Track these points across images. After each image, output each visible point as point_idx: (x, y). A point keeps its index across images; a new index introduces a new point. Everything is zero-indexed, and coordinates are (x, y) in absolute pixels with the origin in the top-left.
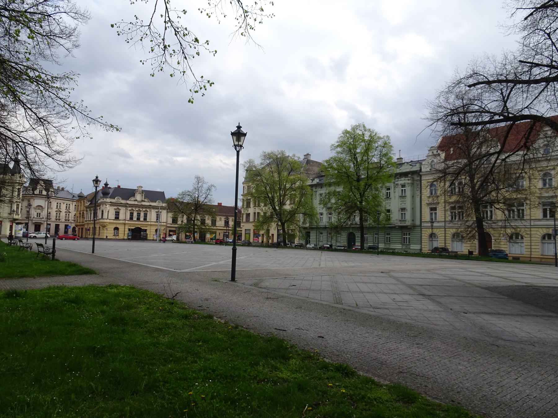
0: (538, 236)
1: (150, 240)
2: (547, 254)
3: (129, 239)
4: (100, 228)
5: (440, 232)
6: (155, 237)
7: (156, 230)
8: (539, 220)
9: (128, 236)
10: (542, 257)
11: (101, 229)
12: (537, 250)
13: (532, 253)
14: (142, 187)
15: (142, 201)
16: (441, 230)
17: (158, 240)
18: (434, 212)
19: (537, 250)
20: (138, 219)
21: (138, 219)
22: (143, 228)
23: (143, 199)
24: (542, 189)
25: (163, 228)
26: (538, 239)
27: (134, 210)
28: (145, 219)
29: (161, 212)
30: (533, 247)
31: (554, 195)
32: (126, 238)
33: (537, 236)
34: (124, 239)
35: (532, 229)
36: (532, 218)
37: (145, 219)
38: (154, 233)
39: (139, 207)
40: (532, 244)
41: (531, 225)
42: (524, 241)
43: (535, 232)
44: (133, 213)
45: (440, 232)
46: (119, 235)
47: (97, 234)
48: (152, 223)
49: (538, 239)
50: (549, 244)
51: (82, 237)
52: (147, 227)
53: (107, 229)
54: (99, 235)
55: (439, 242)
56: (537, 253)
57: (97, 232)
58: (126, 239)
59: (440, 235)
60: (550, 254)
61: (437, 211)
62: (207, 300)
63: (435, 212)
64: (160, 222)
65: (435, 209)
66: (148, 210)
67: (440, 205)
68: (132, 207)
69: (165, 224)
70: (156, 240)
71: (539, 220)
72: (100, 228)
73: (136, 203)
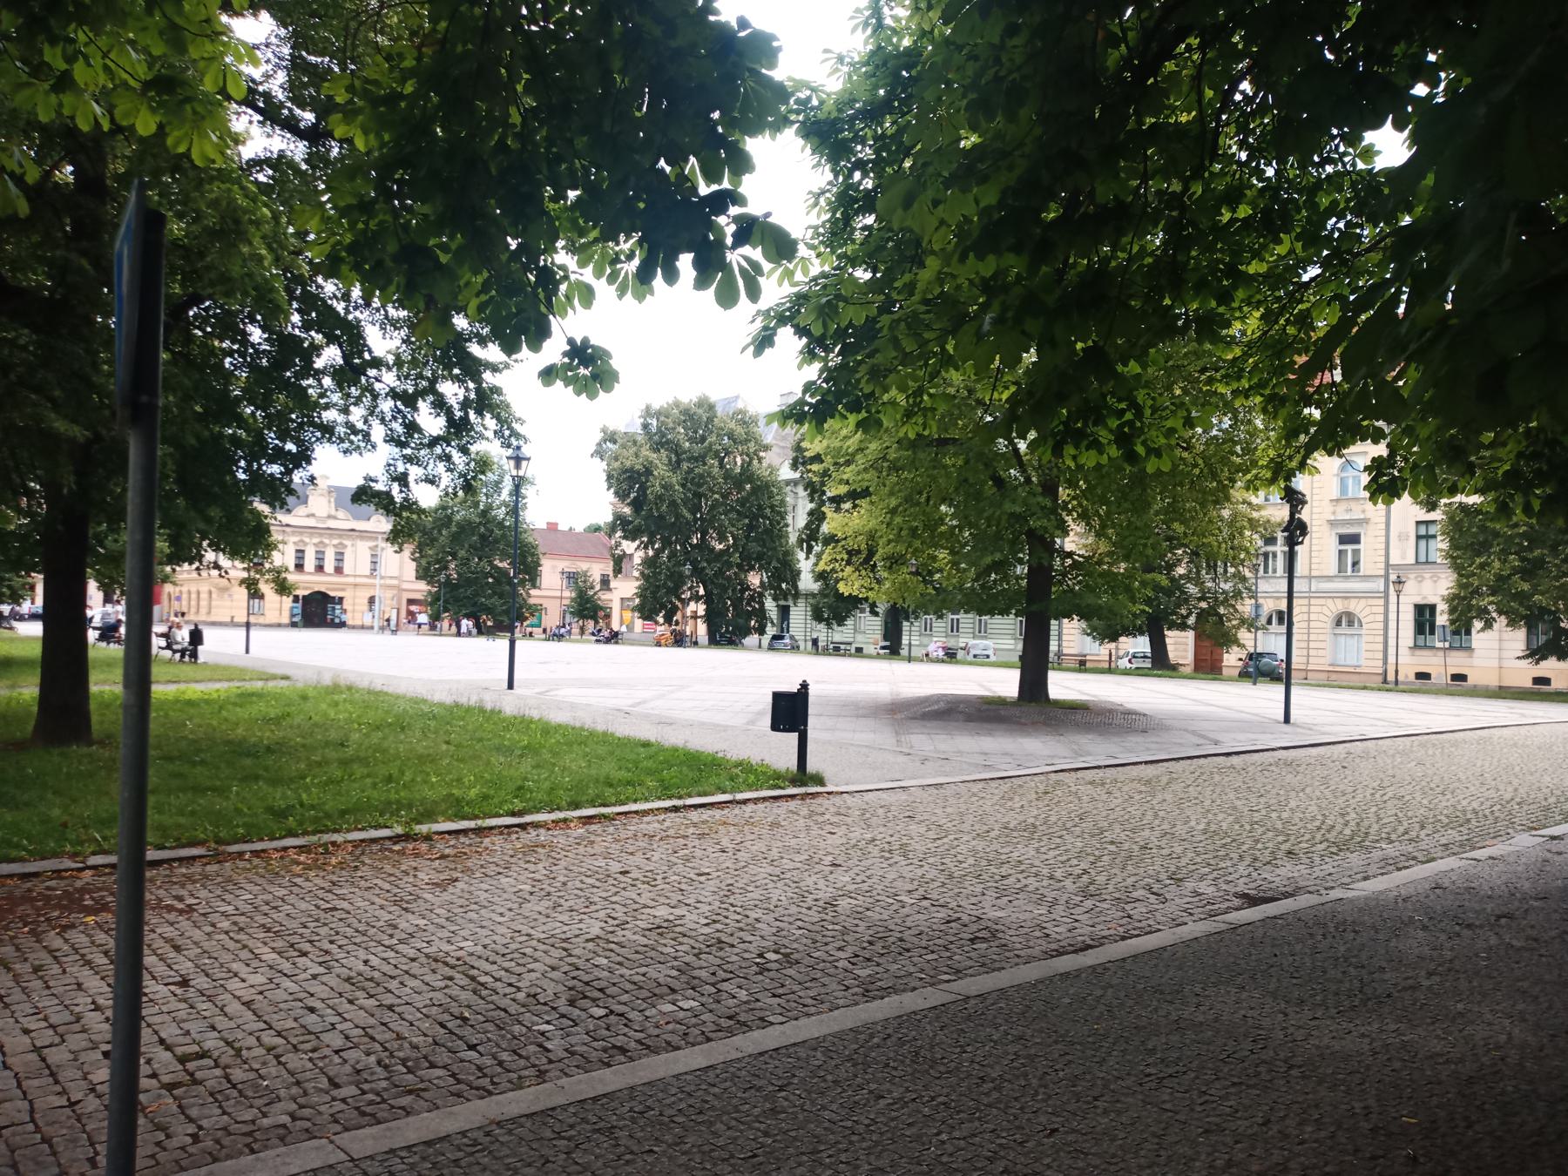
0: (1326, 619)
1: (354, 627)
2: (1342, 663)
3: (294, 625)
4: (210, 593)
5: (1368, 610)
6: (367, 620)
7: (372, 600)
8: (1329, 578)
9: (293, 616)
10: (1331, 669)
11: (214, 596)
12: (1321, 653)
13: (1312, 660)
14: (327, 478)
15: (330, 517)
16: (1371, 602)
17: (376, 628)
18: (1349, 548)
19: (1321, 653)
20: (320, 568)
21: (320, 568)
22: (332, 594)
23: (333, 512)
24: (1337, 500)
25: (389, 594)
26: (1324, 625)
27: (326, 545)
28: (339, 570)
29: (383, 549)
30: (1312, 645)
31: (1362, 517)
32: (286, 620)
33: (1322, 618)
34: (279, 625)
35: (1313, 601)
36: (1314, 573)
37: (339, 570)
38: (366, 607)
39: (321, 535)
40: (1312, 637)
41: (1310, 592)
42: (1363, 632)
43: (1318, 609)
44: (323, 553)
45: (1368, 610)
46: (266, 612)
47: (203, 610)
48: (359, 580)
49: (1324, 625)
50: (1348, 639)
51: (760, 646)
52: (343, 590)
53: (230, 596)
54: (209, 613)
55: (1365, 639)
56: (1322, 661)
57: (204, 603)
58: (286, 626)
59: (1370, 618)
60: (1348, 663)
61: (1361, 546)
62: (277, 721)
63: (1355, 547)
64: (382, 578)
65: (1354, 539)
66: (345, 542)
67: (1371, 527)
68: (301, 533)
69: (395, 582)
70: (372, 628)
71: (1329, 578)
72: (210, 593)
73: (311, 522)
